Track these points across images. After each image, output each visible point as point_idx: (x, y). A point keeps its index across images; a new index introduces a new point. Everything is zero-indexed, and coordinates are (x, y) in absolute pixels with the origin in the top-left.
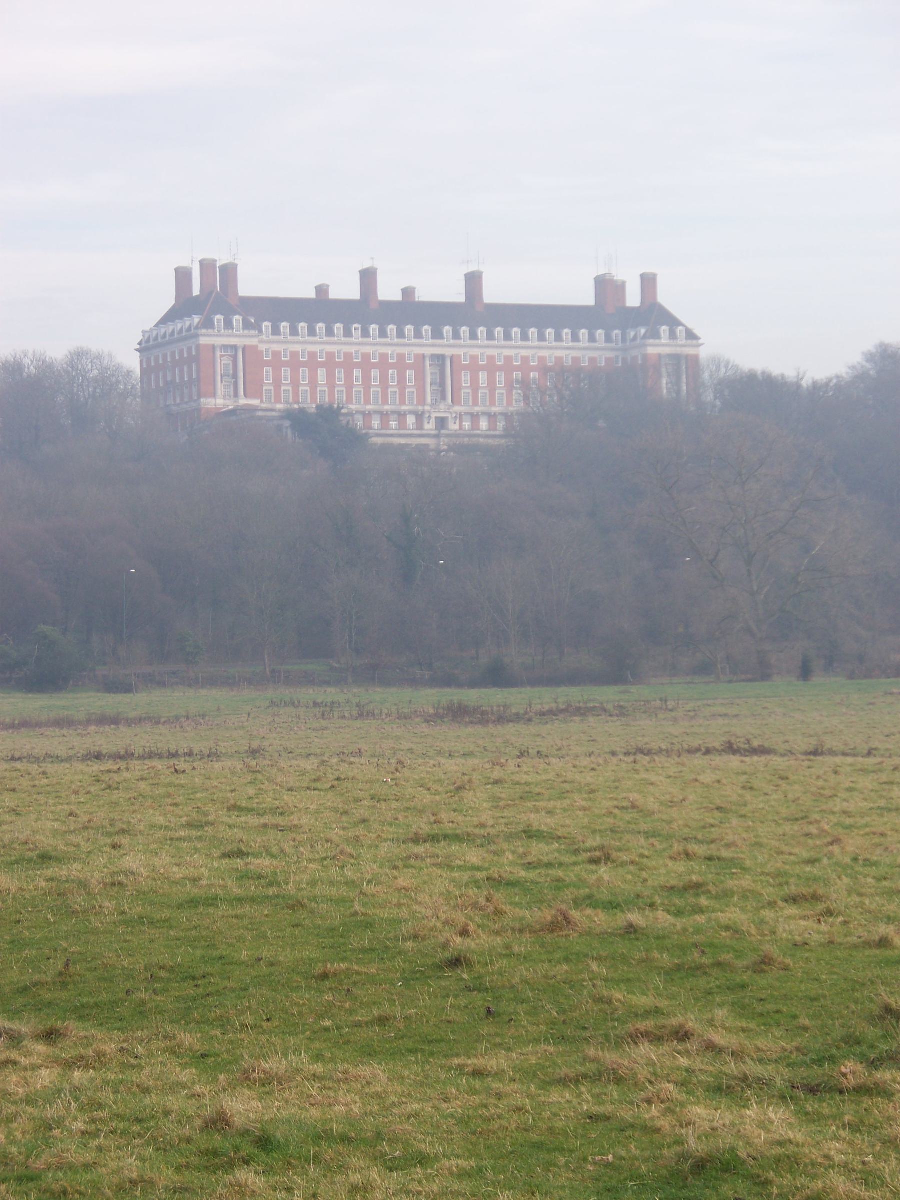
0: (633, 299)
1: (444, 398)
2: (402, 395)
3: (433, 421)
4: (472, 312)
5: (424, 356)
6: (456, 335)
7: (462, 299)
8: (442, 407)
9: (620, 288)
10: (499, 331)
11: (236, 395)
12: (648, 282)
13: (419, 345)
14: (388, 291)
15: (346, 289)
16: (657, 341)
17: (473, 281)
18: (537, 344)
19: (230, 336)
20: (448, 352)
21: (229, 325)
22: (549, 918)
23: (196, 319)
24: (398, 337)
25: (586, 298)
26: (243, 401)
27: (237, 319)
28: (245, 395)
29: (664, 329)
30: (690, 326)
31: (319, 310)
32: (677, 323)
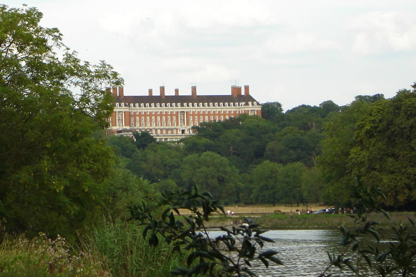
0: (243, 93)
1: (184, 124)
3: (181, 131)
4: (194, 99)
5: (178, 112)
6: (188, 106)
8: (184, 126)
9: (239, 89)
10: (216, 104)
11: (122, 125)
12: (247, 88)
15: (156, 93)
16: (248, 106)
17: (194, 89)
18: (154, 108)
20: (185, 110)
21: (120, 105)
24: (228, 106)
25: (229, 93)
26: (124, 127)
27: (123, 104)
28: (125, 125)
29: (250, 103)
30: (258, 101)
31: (150, 99)
32: (255, 101)
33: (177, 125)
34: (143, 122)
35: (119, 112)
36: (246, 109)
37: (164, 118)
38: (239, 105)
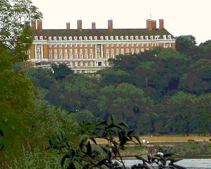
1: (101, 56)
2: (89, 56)
4: (110, 32)
7: (107, 28)
12: (162, 22)
13: (93, 41)
14: (86, 26)
19: (100, 42)
21: (39, 38)
22: (179, 85)
23: (159, 36)
25: (144, 27)
26: (43, 60)
28: (44, 57)
29: (165, 36)
31: (67, 33)
33: (94, 57)
34: (51, 55)
35: (38, 45)
36: (160, 42)
37: (81, 50)
38: (154, 39)
